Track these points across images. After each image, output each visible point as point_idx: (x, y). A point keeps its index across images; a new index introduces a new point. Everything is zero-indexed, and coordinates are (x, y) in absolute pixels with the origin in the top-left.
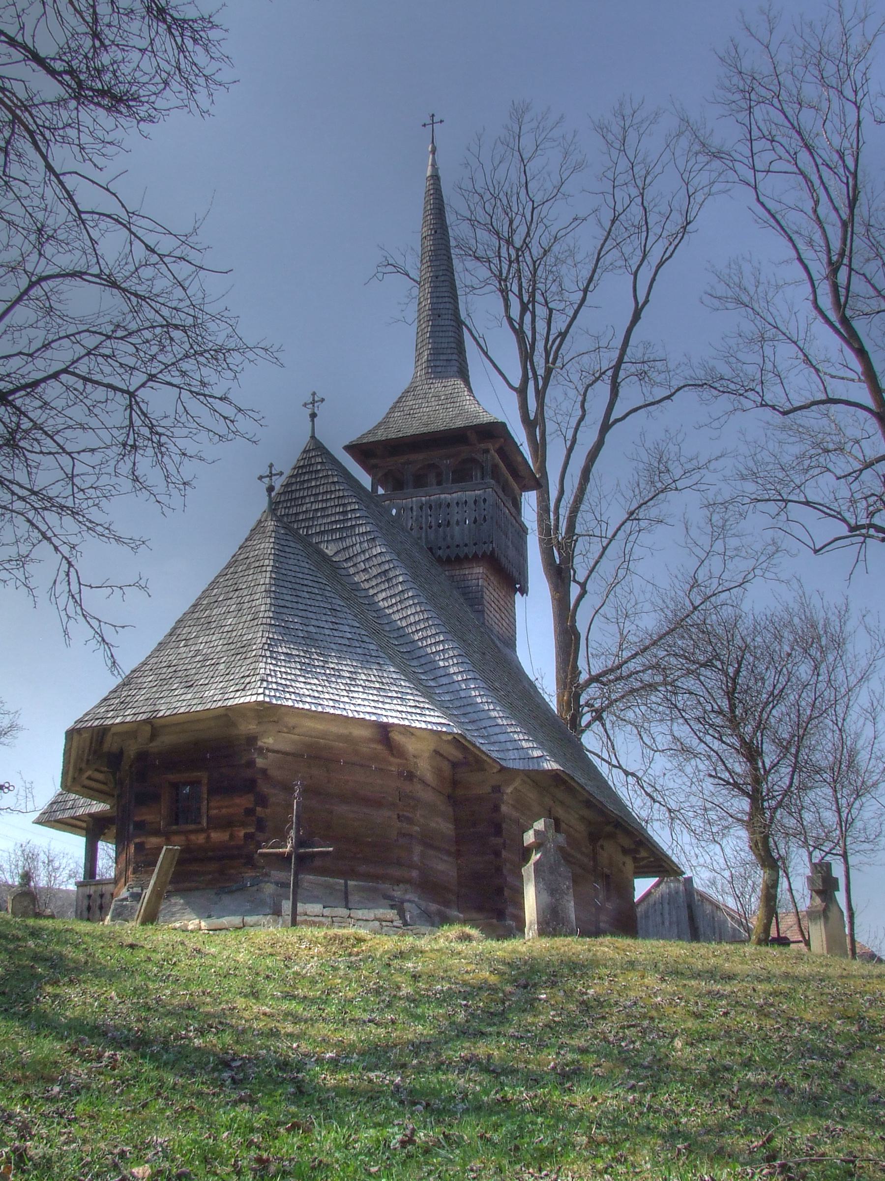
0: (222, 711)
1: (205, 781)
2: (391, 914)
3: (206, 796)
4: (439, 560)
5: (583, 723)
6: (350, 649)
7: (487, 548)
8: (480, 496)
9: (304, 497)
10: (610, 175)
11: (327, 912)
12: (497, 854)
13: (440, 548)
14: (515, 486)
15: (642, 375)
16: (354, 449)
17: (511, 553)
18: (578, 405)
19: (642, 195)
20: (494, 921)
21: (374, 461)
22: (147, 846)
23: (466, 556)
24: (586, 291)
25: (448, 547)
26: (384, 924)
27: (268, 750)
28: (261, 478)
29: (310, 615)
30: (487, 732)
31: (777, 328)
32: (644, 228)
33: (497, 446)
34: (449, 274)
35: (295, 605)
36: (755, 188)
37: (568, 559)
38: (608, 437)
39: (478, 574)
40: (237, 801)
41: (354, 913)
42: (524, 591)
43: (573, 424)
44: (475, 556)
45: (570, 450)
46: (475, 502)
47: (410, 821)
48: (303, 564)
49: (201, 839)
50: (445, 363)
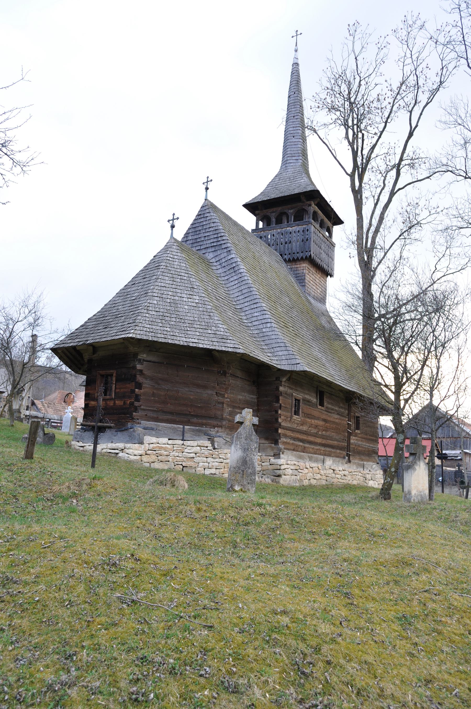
0: (122, 341)
1: (114, 375)
2: (208, 443)
4: (285, 260)
7: (308, 254)
8: (305, 228)
9: (200, 230)
10: (402, 60)
11: (170, 442)
12: (277, 412)
15: (412, 166)
16: (251, 207)
17: (324, 256)
18: (382, 181)
19: (416, 70)
20: (273, 445)
21: (257, 212)
23: (298, 258)
24: (386, 123)
27: (144, 360)
29: (179, 291)
33: (316, 202)
35: (170, 286)
37: (370, 257)
39: (305, 267)
40: (128, 385)
41: (186, 443)
45: (376, 204)
46: (303, 231)
47: (223, 396)
48: (182, 265)
49: (111, 403)
50: (295, 161)
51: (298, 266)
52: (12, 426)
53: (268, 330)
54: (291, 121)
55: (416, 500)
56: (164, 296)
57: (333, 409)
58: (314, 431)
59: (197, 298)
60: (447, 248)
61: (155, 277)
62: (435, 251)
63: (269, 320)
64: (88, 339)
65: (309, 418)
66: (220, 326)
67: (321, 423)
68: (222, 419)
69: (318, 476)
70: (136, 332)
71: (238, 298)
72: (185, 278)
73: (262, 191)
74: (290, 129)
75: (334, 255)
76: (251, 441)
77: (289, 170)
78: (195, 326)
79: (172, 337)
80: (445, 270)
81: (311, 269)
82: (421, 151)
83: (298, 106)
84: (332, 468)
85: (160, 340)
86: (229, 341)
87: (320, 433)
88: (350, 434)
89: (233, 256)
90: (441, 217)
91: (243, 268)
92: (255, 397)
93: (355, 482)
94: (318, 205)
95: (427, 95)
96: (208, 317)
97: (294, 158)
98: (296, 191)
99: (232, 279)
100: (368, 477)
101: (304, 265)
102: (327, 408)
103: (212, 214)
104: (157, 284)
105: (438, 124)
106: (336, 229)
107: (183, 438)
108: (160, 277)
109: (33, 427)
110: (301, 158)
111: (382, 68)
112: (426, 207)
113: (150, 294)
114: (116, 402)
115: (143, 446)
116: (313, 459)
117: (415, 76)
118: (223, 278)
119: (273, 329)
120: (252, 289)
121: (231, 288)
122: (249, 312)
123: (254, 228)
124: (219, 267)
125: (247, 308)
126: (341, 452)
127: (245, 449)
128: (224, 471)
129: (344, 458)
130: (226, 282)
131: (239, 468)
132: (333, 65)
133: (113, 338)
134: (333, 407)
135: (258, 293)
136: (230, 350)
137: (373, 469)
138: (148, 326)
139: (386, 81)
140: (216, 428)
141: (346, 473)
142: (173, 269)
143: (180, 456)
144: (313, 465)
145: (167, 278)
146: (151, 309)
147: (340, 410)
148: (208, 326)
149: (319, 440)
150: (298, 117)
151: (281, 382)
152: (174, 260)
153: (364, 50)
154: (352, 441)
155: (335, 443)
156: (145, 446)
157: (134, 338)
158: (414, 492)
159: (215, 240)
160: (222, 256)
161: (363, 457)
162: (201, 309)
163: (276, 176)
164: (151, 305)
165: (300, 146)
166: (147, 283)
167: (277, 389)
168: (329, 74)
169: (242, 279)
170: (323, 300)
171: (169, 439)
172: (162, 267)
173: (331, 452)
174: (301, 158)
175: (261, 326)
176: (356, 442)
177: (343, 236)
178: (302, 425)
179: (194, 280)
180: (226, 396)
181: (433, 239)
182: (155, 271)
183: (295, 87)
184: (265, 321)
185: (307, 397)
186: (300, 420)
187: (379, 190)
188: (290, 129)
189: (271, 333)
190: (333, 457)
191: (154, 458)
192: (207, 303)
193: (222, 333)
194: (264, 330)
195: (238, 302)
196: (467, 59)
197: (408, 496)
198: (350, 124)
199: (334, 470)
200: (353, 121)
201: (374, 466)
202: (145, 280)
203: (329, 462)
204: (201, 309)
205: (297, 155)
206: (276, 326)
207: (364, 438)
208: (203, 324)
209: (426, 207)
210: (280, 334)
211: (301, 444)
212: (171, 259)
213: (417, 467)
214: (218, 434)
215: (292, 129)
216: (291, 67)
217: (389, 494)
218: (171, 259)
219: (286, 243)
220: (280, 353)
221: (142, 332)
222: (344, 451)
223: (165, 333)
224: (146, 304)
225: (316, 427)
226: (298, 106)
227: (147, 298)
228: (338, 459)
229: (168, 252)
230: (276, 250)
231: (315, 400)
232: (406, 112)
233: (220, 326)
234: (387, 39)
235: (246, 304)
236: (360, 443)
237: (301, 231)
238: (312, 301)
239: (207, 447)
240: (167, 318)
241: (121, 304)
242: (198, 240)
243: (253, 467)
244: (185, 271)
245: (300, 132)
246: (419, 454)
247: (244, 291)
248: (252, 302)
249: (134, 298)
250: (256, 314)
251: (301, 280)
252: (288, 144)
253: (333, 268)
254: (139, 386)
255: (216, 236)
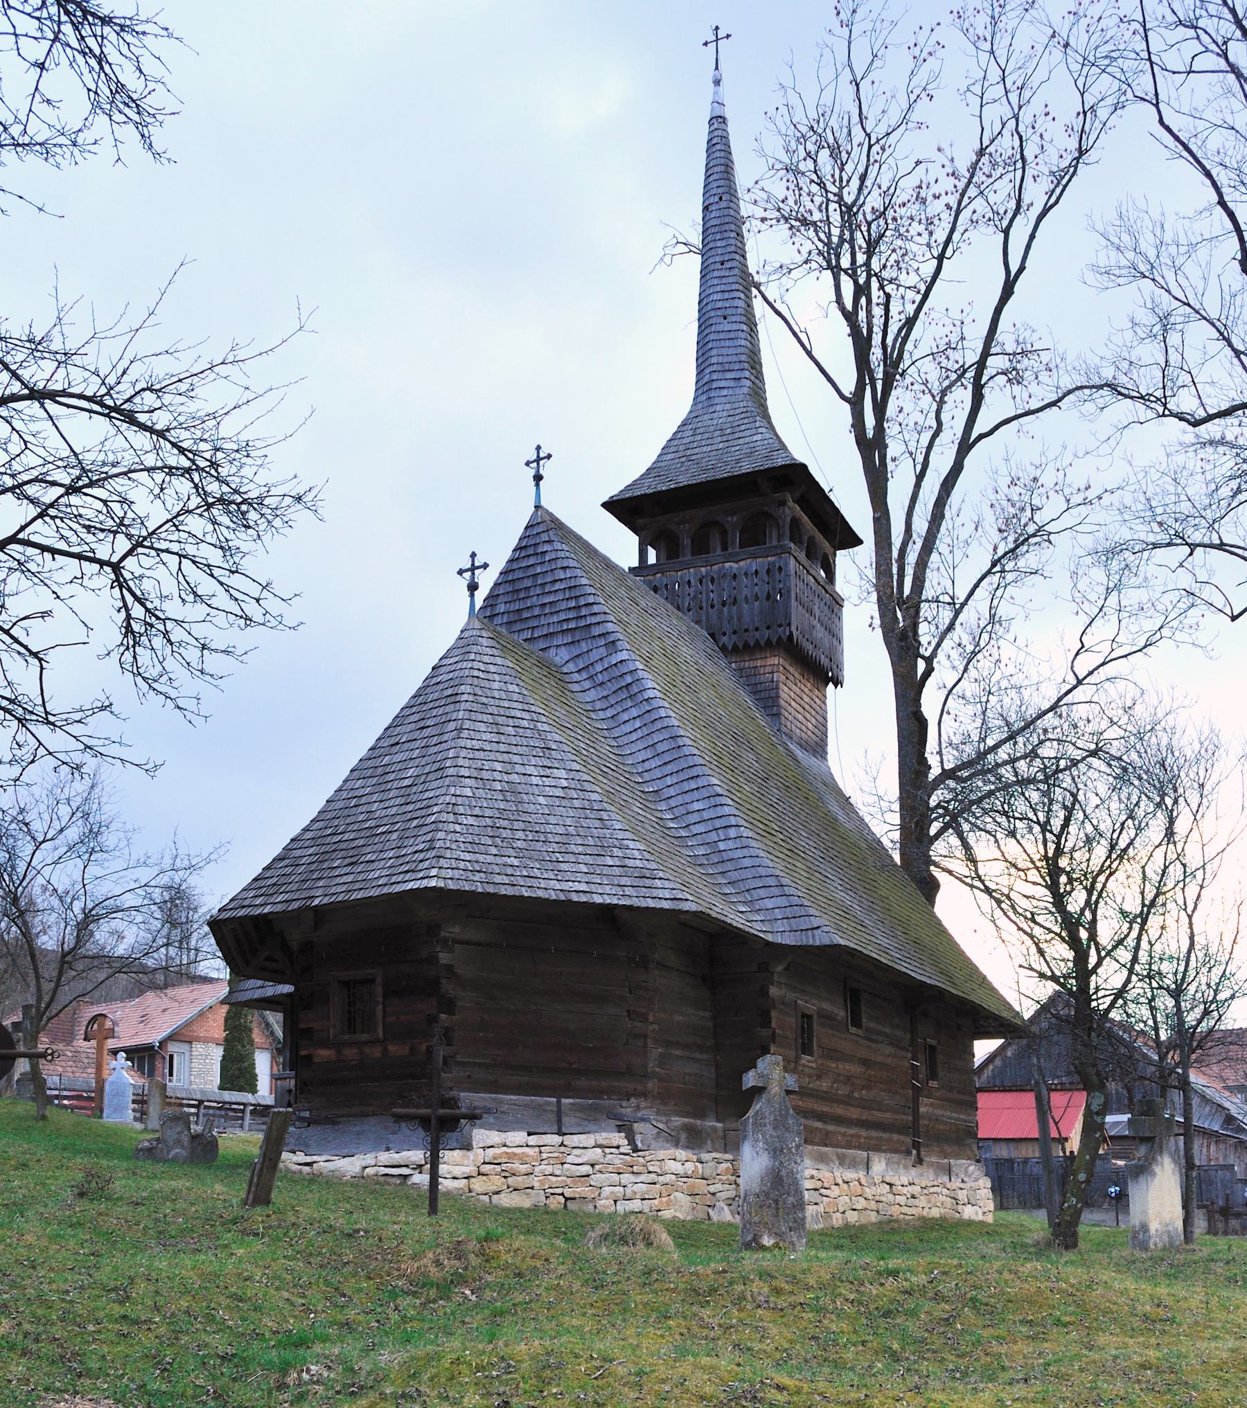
1: (379, 980)
2: (619, 1138)
3: (381, 1000)
4: (723, 649)
5: (933, 832)
6: (564, 803)
7: (783, 632)
8: (773, 563)
10: (977, 89)
11: (533, 1140)
13: (724, 634)
14: (826, 545)
15: (1014, 377)
16: (624, 508)
17: (820, 633)
18: (932, 415)
21: (640, 521)
22: (316, 1060)
23: (757, 644)
25: (735, 632)
26: (607, 1150)
27: (455, 941)
28: (461, 572)
29: (516, 759)
30: (751, 896)
31: (1189, 305)
32: (1019, 165)
33: (797, 495)
34: (737, 257)
36: (1157, 105)
38: (968, 462)
39: (775, 665)
42: (837, 682)
43: (925, 441)
44: (769, 643)
45: (920, 477)
46: (768, 571)
47: (644, 1019)
48: (511, 688)
49: (376, 1052)
50: (732, 384)
51: (759, 663)
52: (44, 1117)
53: (731, 845)
54: (716, 274)
55: (1160, 1245)
56: (485, 775)
57: (879, 1033)
58: (843, 1091)
59: (563, 774)
60: (1109, 591)
61: (452, 726)
62: (1079, 599)
63: (733, 821)
64: (312, 893)
65: (831, 1058)
66: (631, 844)
67: (856, 1069)
68: (646, 1076)
69: (861, 1203)
70: (443, 873)
71: (647, 765)
72: (525, 724)
73: (649, 465)
74: (715, 297)
75: (841, 629)
76: (787, 1129)
77: (718, 408)
78: (573, 848)
79: (530, 882)
80: (1106, 648)
81: (791, 670)
82: (1035, 336)
83: (733, 235)
84: (888, 1179)
85: (503, 891)
86: (658, 883)
87: (856, 1095)
88: (917, 1092)
89: (624, 655)
90: (1097, 514)
91: (652, 685)
92: (708, 1014)
93: (935, 1213)
94: (800, 501)
95: (1046, 184)
96: (597, 824)
97: (729, 375)
98: (746, 467)
99: (625, 717)
100: (962, 1195)
101: (775, 661)
102: (867, 1029)
103: (558, 546)
104: (462, 743)
105: (1090, 277)
106: (843, 559)
107: (560, 1128)
108: (467, 724)
109: (274, 1127)
110: (747, 374)
111: (922, 111)
112: (1057, 488)
113: (451, 771)
114: (390, 1048)
115: (471, 1154)
116: (847, 1161)
117: (1016, 136)
118: (602, 715)
119: (745, 842)
120: (680, 742)
121: (626, 740)
122: (680, 800)
123: (636, 564)
124: (587, 685)
125: (672, 791)
126: (902, 1138)
127: (775, 1150)
128: (661, 1202)
129: (908, 1153)
130: (612, 724)
131: (767, 1195)
132: (794, 100)
133: (385, 890)
134: (880, 1027)
135: (696, 752)
136: (666, 905)
137: (970, 1176)
138: (468, 856)
139: (939, 150)
140: (632, 1100)
141: (916, 1190)
142: (492, 702)
143: (557, 1173)
144: (850, 1175)
145: (482, 727)
146: (461, 810)
147: (901, 1032)
148: (602, 849)
149: (854, 1113)
150: (734, 264)
151: (772, 973)
152: (490, 676)
153: (877, 63)
154: (922, 1110)
155: (887, 1116)
156: (476, 1155)
157: (441, 888)
158: (1154, 1227)
159: (571, 615)
160: (595, 655)
161: (948, 1149)
162: (576, 803)
163: (684, 424)
164: (460, 800)
165: (743, 342)
166: (435, 740)
167: (764, 992)
168: (782, 122)
169: (654, 716)
170: (819, 748)
171: (529, 1134)
172: (465, 697)
173: (880, 1139)
174: (747, 374)
175: (713, 836)
176: (931, 1110)
177: (853, 571)
178: (819, 1077)
179: (546, 727)
180: (651, 1018)
181: (1073, 568)
182: (448, 709)
183: (721, 183)
184: (722, 822)
185: (826, 1006)
186: (814, 1065)
187: (926, 437)
188: (715, 297)
189: (739, 853)
190: (885, 1151)
191: (497, 1182)
192: (587, 786)
193: (638, 863)
194: (722, 846)
195: (647, 776)
196: (1157, 105)
197: (1141, 1236)
198: (845, 262)
199: (891, 1185)
200: (853, 255)
201: (972, 1168)
202: (426, 732)
203: (879, 1165)
204: (576, 803)
205: (737, 366)
206: (751, 834)
207: (947, 1100)
208: (591, 841)
209: (1057, 488)
210: (762, 854)
211: (819, 1125)
212: (481, 675)
213: (1157, 1169)
214: (640, 1115)
215: (719, 296)
216: (706, 129)
217: (1075, 1235)
218: (481, 675)
219: (724, 604)
220: (769, 904)
221: (457, 874)
222: (907, 1135)
223: (509, 871)
224: (448, 799)
225: (848, 1079)
226: (733, 235)
227: (447, 781)
228: (896, 1157)
229: (472, 656)
230: (697, 622)
231: (842, 1013)
232: (992, 229)
233: (631, 844)
234: (938, 35)
235: (669, 781)
236: (939, 1112)
237: (763, 572)
238: (799, 753)
239: (618, 1147)
240: (505, 834)
241: (375, 797)
242: (525, 615)
243: (796, 1191)
244: (520, 706)
245: (741, 303)
246: (1161, 1139)
247: (661, 748)
248: (682, 776)
249: (406, 782)
250: (696, 806)
251: (768, 701)
252: (712, 337)
253: (842, 664)
254: (449, 1006)
255: (573, 604)
